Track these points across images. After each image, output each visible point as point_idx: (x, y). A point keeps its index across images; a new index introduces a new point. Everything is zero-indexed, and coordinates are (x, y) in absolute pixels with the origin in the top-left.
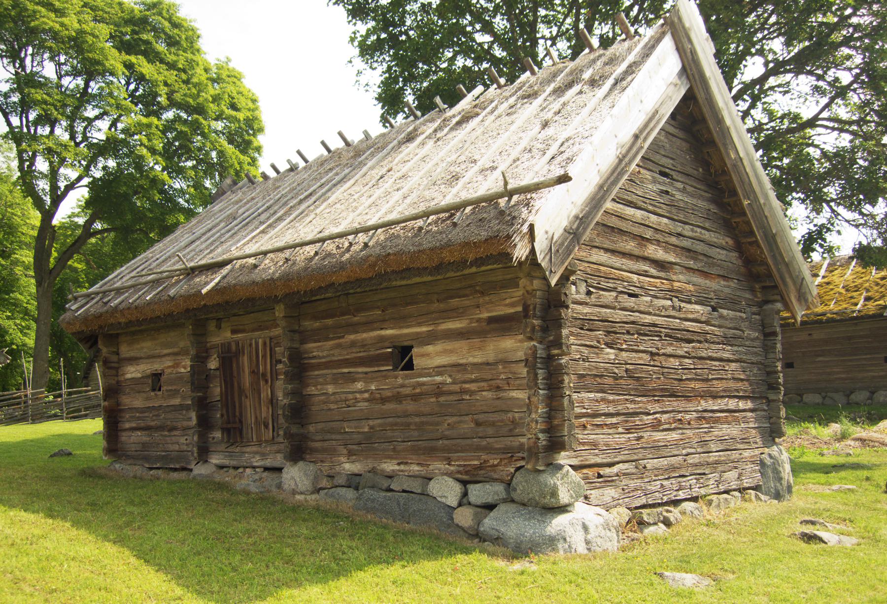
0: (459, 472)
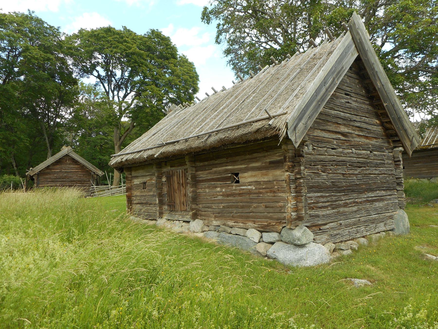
0: (258, 227)
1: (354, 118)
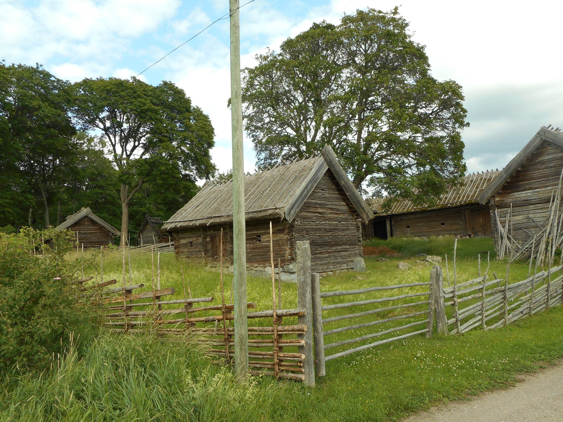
1: (327, 203)
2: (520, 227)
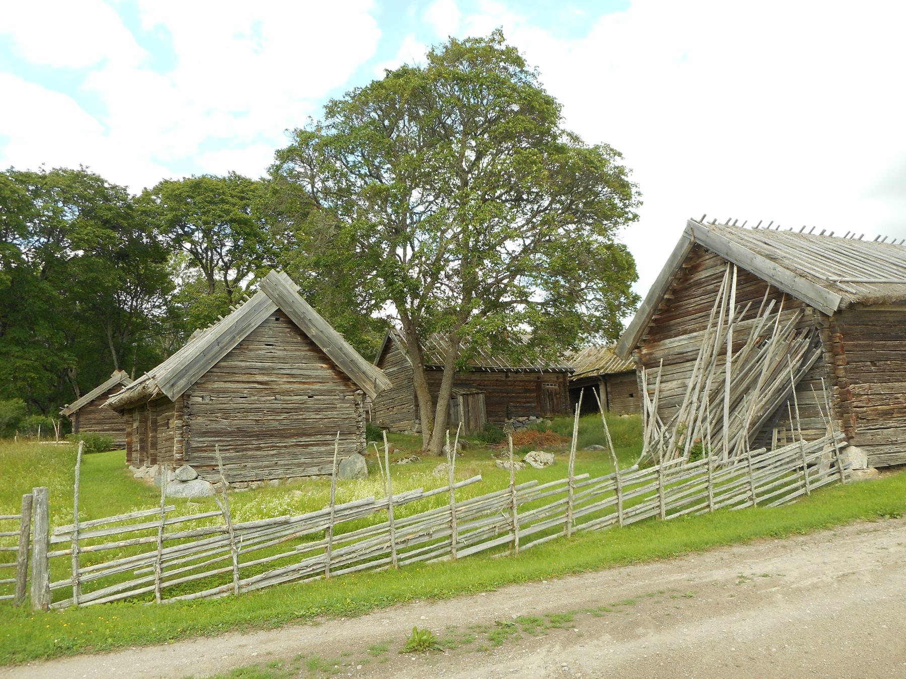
2: (673, 401)
